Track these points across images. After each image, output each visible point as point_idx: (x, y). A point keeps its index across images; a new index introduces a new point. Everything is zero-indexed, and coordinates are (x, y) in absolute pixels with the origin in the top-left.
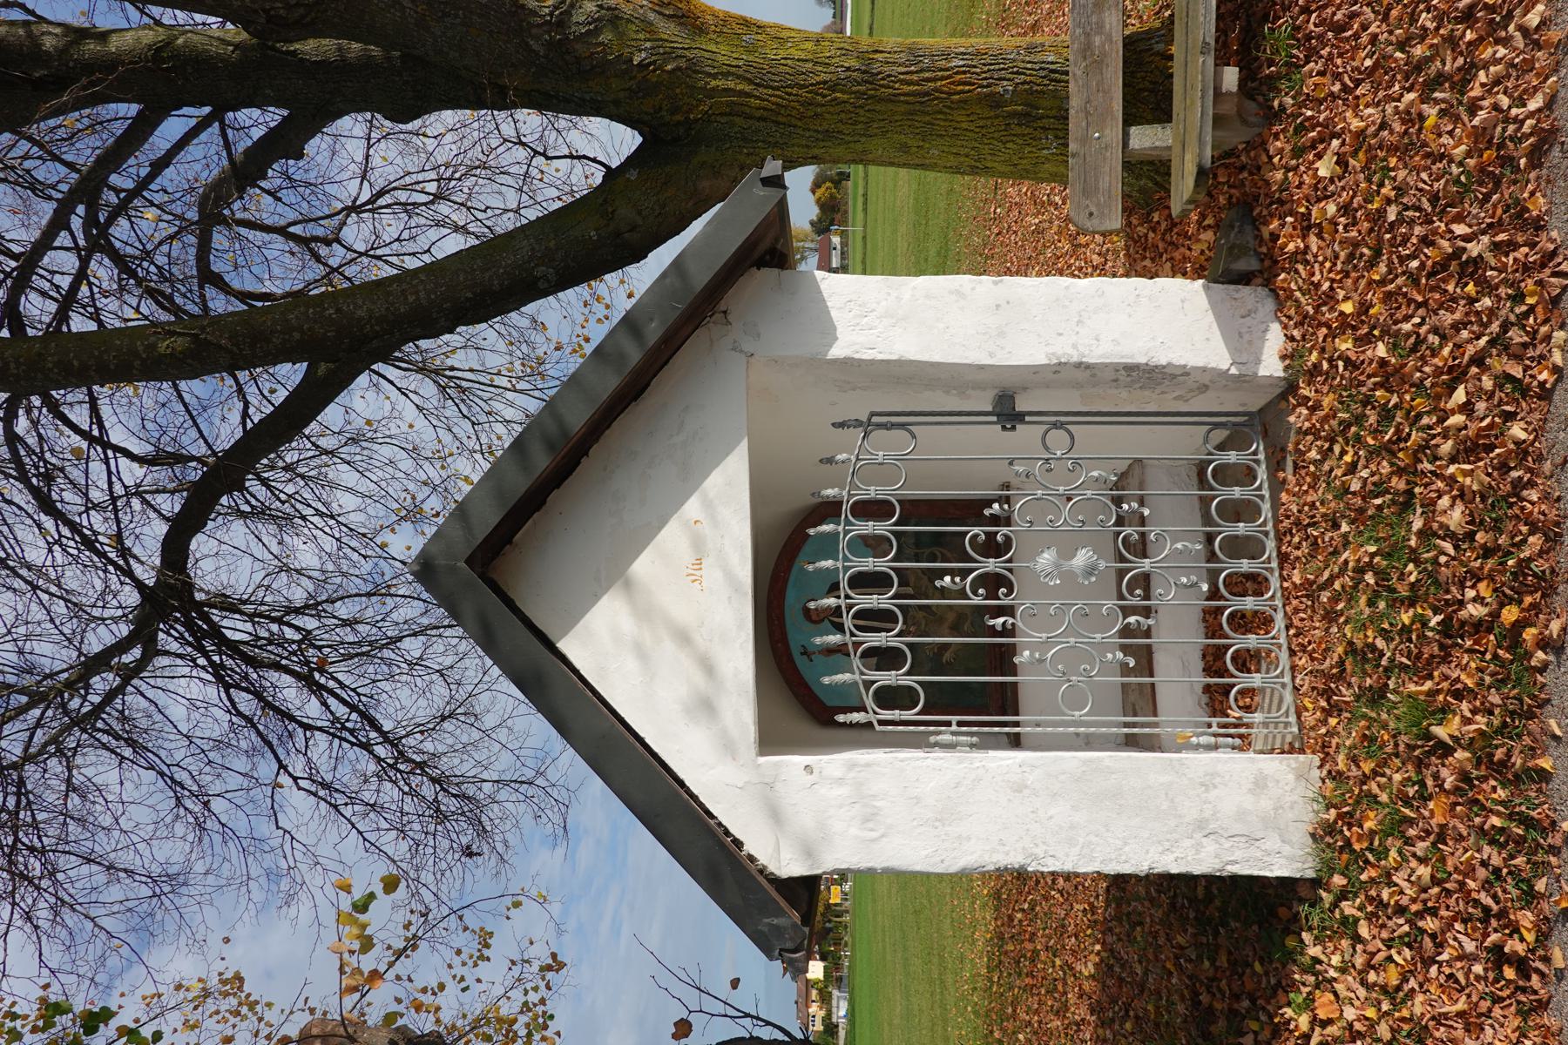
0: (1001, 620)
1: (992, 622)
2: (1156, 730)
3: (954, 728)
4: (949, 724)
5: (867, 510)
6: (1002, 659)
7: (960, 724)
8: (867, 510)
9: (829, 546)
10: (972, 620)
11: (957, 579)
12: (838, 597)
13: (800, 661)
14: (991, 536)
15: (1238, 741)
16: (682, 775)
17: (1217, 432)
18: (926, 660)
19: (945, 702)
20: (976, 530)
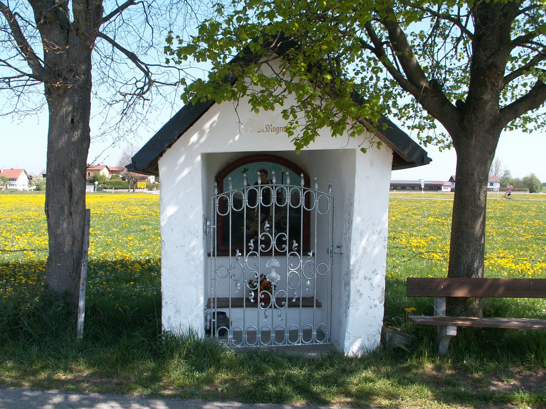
0: (252, 245)
1: (252, 241)
2: (212, 335)
3: (212, 226)
4: (214, 318)
5: (308, 197)
6: (238, 245)
7: (214, 322)
8: (308, 197)
9: (295, 182)
10: (253, 235)
11: (268, 229)
12: (276, 183)
13: (242, 168)
14: (285, 242)
15: (208, 328)
16: (194, 125)
17: (115, 51)
18: (237, 217)
19: (222, 222)
20: (287, 237)
